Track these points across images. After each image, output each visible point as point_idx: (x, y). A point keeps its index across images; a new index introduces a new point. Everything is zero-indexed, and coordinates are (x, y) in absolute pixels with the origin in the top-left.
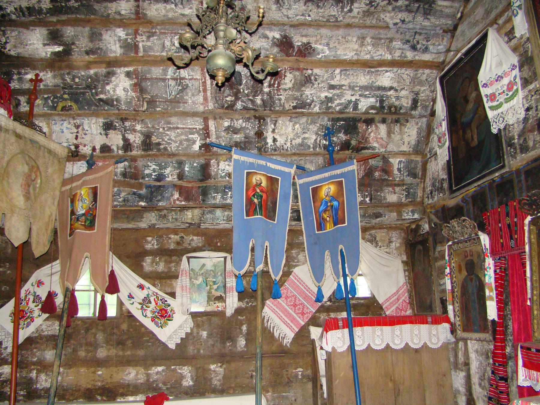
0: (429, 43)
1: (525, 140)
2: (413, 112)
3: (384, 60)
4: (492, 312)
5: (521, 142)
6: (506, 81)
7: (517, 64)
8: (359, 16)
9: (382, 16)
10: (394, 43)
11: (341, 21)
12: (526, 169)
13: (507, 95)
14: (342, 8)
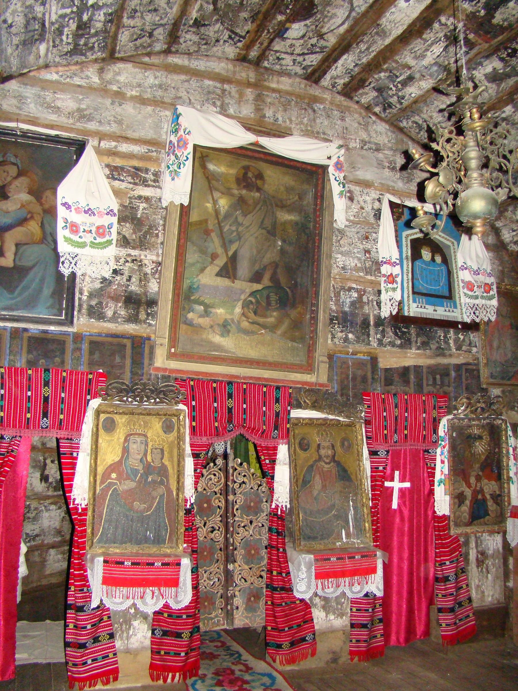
1: (100, 303)
5: (93, 303)
7: (116, 211)
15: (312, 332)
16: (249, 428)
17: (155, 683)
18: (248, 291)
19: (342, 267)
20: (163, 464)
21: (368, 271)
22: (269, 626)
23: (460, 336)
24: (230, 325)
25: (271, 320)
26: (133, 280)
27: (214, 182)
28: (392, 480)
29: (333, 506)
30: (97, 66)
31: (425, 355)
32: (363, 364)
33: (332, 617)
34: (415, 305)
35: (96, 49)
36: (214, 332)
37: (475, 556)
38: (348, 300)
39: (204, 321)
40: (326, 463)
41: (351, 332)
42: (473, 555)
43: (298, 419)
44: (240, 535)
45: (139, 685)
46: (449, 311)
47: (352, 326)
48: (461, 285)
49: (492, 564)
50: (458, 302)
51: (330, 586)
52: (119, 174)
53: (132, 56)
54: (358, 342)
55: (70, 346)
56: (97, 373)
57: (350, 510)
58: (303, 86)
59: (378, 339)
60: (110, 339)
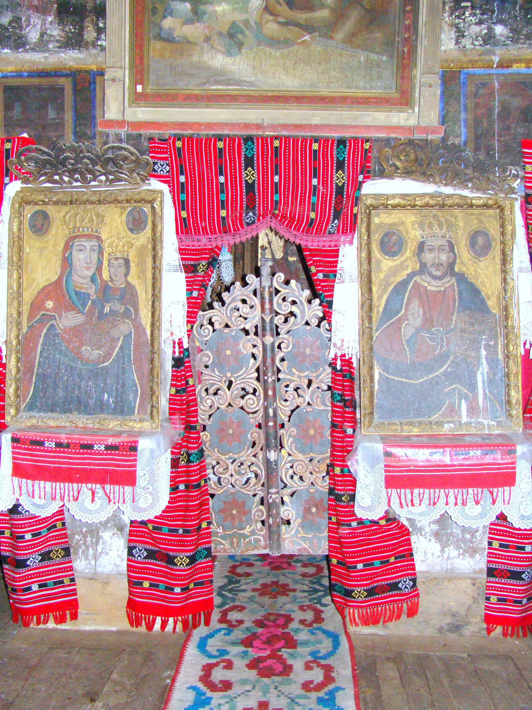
1: (17, 20)
15: (407, 28)
16: (282, 217)
17: (134, 629)
20: (128, 283)
22: (335, 557)
24: (242, 33)
29: (444, 357)
32: (524, 83)
33: (452, 552)
36: (212, 47)
40: (435, 278)
41: (500, 21)
43: (376, 196)
44: (288, 403)
45: (114, 629)
47: (502, 10)
51: (416, 501)
54: (515, 41)
56: (19, 139)
57: (479, 364)
60: (36, 81)
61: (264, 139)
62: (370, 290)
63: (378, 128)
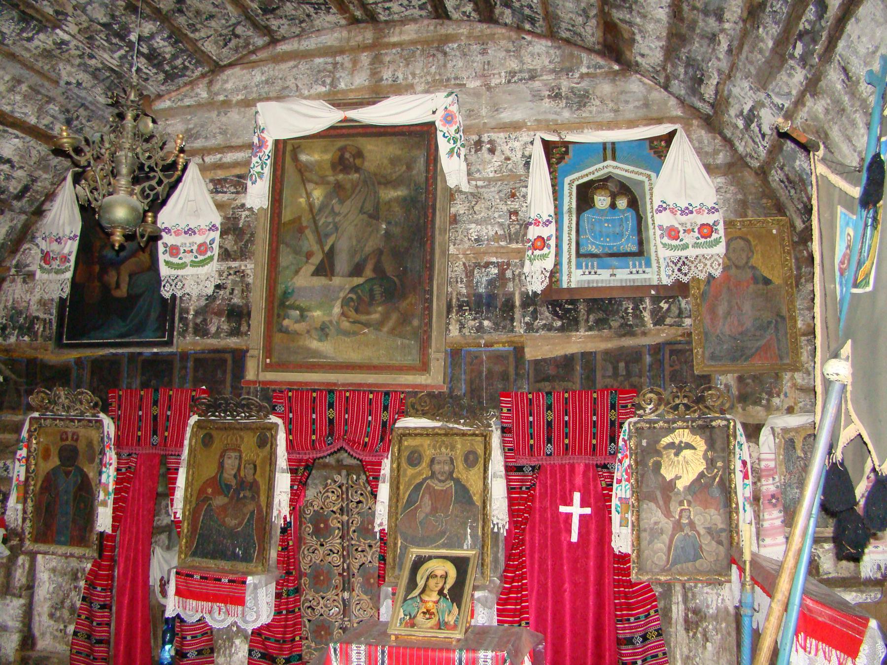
0: (88, 124)
1: (205, 320)
2: (15, 203)
3: (25, 122)
4: (104, 520)
5: (198, 321)
6: (199, 239)
7: (218, 225)
8: (34, 51)
9: (61, 66)
10: (51, 106)
11: (7, 45)
12: (198, 356)
13: (196, 257)
14: (23, 30)
15: (426, 324)
18: (348, 287)
19: (475, 240)
20: (255, 480)
21: (511, 238)
23: (662, 304)
25: (375, 316)
26: (236, 292)
27: (307, 174)
28: (570, 503)
30: (206, 80)
31: (601, 337)
34: (580, 272)
35: (191, 67)
37: (682, 614)
38: (485, 279)
39: (300, 327)
40: (440, 481)
41: (487, 318)
42: (678, 611)
46: (638, 272)
47: (488, 311)
48: (658, 232)
49: (715, 629)
50: (653, 257)
52: (222, 187)
53: (241, 58)
55: (177, 365)
57: (466, 538)
58: (432, 28)
59: (527, 323)
61: (340, 391)
62: (398, 488)
63: (408, 386)
